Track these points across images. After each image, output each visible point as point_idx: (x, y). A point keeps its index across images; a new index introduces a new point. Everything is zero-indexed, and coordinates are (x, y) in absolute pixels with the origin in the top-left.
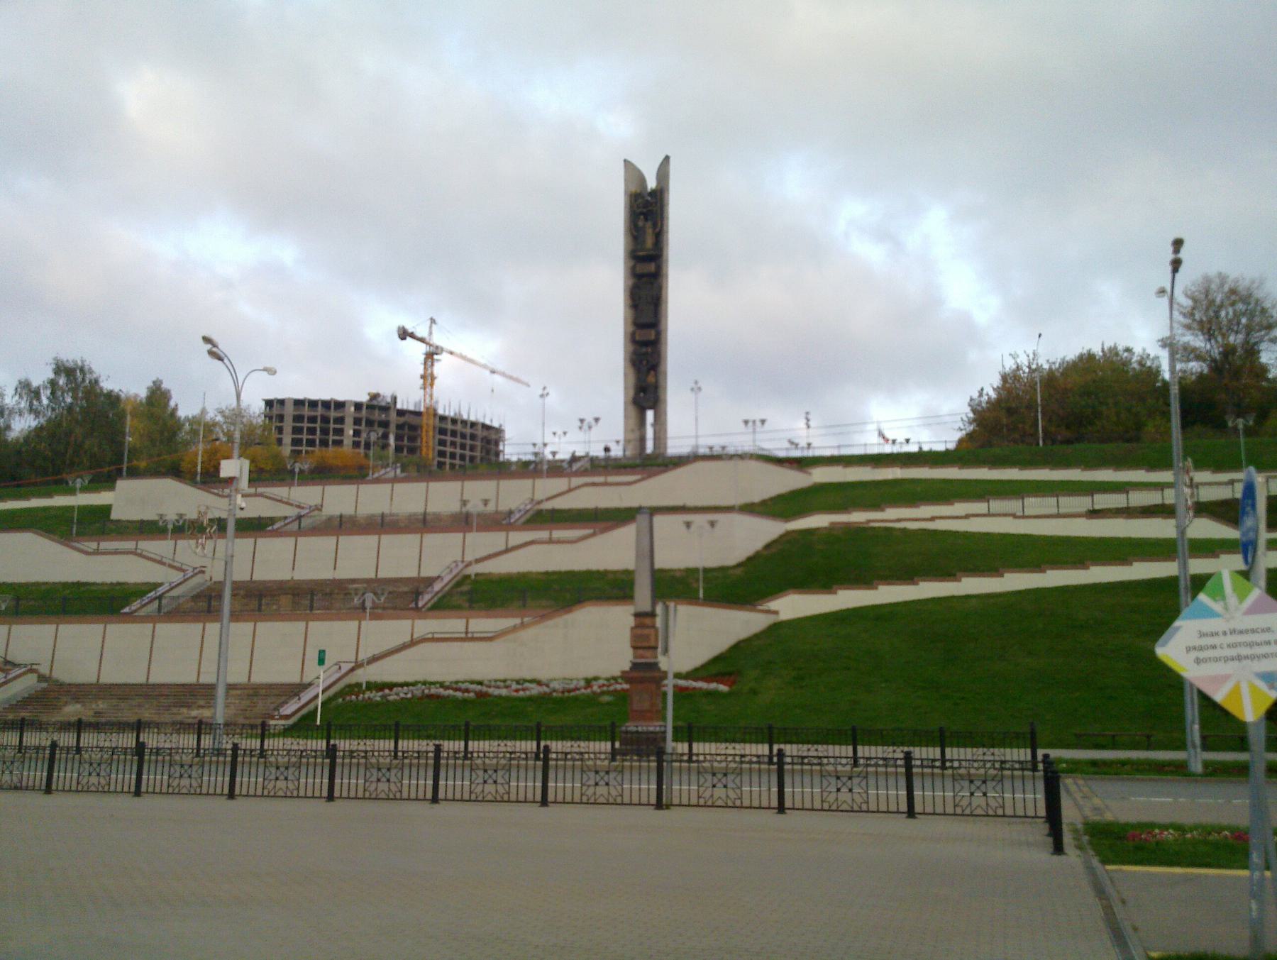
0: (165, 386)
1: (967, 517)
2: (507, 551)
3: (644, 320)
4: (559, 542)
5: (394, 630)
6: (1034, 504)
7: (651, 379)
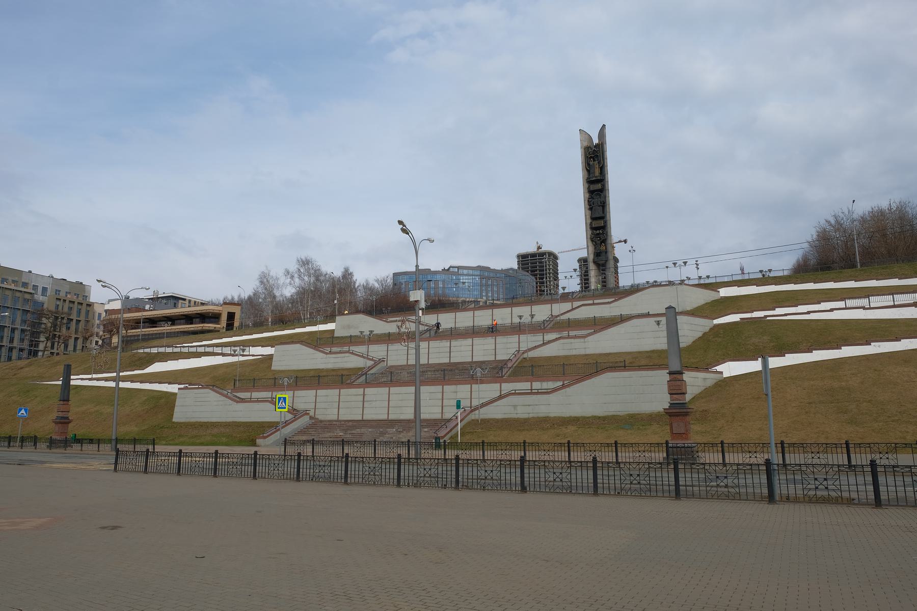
0: (351, 270)
1: (832, 310)
2: (544, 344)
3: (597, 215)
4: (549, 342)
5: (490, 390)
6: (876, 301)
7: (603, 248)
